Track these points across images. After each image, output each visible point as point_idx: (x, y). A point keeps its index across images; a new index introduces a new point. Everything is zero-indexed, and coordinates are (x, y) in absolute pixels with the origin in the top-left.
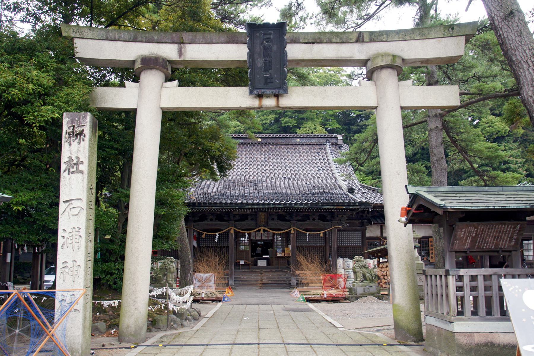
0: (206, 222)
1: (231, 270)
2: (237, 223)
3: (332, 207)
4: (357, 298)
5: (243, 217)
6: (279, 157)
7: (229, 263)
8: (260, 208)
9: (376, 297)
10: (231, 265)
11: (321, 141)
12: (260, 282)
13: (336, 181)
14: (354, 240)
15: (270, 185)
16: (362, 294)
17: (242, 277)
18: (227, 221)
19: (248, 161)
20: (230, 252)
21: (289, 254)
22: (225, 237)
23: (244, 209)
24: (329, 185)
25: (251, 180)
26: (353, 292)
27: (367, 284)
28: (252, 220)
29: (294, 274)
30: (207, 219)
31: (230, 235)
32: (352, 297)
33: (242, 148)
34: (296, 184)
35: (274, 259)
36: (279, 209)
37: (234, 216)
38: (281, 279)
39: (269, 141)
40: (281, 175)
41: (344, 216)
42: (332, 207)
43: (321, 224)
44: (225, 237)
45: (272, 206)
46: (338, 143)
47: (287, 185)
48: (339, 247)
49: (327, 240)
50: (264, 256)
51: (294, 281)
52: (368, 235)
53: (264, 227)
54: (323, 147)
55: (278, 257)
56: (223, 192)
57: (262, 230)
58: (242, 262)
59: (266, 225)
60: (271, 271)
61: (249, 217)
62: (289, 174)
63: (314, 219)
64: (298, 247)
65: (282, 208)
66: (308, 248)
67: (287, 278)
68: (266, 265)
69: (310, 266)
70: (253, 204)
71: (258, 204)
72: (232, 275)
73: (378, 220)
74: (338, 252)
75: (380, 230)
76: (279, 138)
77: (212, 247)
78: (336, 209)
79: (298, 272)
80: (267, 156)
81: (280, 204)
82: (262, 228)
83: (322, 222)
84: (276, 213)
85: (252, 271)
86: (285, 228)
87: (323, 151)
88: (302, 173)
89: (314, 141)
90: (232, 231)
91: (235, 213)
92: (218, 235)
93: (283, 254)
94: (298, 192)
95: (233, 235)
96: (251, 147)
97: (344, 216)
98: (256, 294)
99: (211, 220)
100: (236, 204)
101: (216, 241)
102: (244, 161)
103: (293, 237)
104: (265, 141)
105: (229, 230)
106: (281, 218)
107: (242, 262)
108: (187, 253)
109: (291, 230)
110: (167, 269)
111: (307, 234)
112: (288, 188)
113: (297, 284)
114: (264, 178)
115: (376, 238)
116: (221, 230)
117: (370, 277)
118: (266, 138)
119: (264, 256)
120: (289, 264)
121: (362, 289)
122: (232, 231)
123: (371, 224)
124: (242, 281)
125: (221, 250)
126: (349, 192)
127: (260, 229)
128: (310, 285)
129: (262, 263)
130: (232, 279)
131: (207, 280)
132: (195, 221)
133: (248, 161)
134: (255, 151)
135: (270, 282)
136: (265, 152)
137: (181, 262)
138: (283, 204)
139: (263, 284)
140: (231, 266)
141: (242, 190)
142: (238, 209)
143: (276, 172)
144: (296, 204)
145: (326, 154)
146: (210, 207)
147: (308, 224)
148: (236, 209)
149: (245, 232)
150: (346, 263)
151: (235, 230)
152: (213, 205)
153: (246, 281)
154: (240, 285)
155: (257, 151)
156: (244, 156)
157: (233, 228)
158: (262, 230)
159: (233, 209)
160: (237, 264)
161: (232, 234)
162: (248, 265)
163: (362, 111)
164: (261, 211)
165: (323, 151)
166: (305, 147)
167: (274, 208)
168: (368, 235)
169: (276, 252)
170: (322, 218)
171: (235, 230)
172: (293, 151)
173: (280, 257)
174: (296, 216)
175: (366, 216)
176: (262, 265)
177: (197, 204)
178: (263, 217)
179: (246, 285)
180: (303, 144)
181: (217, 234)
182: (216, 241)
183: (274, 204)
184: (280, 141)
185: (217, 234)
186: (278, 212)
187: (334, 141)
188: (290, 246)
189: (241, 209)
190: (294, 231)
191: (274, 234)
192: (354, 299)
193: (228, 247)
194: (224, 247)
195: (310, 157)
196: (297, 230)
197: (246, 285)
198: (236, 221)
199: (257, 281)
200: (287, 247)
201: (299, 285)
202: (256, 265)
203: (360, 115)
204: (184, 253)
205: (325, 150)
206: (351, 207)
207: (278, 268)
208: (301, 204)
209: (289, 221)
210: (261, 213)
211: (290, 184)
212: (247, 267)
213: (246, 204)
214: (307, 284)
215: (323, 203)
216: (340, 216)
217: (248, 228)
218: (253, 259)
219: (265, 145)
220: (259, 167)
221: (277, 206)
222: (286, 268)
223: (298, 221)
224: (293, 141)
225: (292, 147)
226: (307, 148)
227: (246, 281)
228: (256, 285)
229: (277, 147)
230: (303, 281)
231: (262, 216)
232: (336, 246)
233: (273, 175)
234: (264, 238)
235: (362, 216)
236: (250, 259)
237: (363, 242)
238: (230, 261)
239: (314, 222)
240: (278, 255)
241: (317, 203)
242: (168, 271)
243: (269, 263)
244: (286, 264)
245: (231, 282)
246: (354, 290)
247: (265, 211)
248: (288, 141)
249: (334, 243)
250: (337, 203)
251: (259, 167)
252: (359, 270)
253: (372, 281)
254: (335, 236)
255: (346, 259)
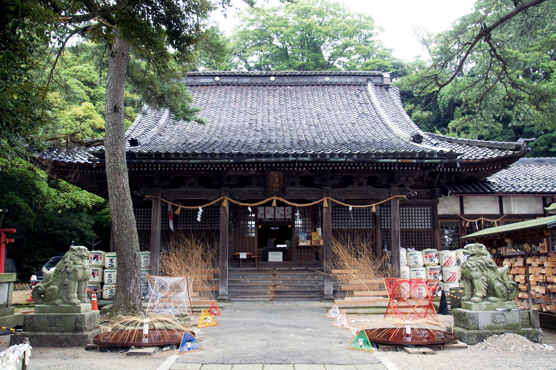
0: (183, 189)
1: (223, 268)
2: (234, 189)
3: (395, 161)
4: (481, 338)
5: (244, 181)
6: (300, 100)
7: (220, 257)
8: (271, 163)
9: (523, 334)
10: (223, 260)
11: (360, 80)
12: (273, 290)
13: (389, 129)
14: (420, 221)
15: (287, 134)
16: (490, 328)
17: (242, 280)
18: (217, 187)
19: (255, 106)
20: (221, 239)
21: (319, 242)
22: (212, 213)
23: (244, 163)
24: (379, 135)
25: (259, 129)
26: (470, 322)
27: (500, 306)
28: (258, 184)
29: (328, 277)
30: (184, 185)
31: (222, 210)
32: (469, 335)
33: (247, 89)
34: (327, 133)
35: (294, 250)
36: (303, 166)
37: (230, 178)
38: (307, 284)
39: (286, 80)
40: (304, 122)
41: (410, 179)
42: (395, 161)
43: (372, 191)
44: (212, 213)
45: (291, 159)
46: (384, 83)
47: (315, 135)
48: (402, 231)
49: (378, 220)
50: (278, 246)
51: (329, 288)
52: (441, 211)
53: (279, 196)
54: (362, 88)
55: (301, 247)
56: (212, 142)
57: (275, 202)
58: (243, 256)
59: (282, 192)
60: (290, 270)
61: (253, 180)
62: (316, 121)
63: (360, 184)
64: (334, 231)
65: (308, 162)
66: (351, 232)
67: (317, 282)
68: (281, 260)
69: (355, 261)
70: (259, 156)
71: (268, 155)
72: (224, 277)
73: (457, 188)
74: (402, 238)
75: (459, 205)
76: (300, 75)
77: (193, 230)
78: (399, 165)
79: (334, 271)
80: (283, 99)
81: (305, 155)
82: (275, 198)
83: (373, 188)
84: (297, 173)
85: (259, 271)
86: (313, 198)
87: (364, 92)
88: (335, 121)
89: (349, 80)
90: (225, 204)
91: (230, 173)
92: (201, 210)
93: (309, 242)
94: (333, 142)
95: (227, 210)
96: (260, 88)
97: (410, 179)
98: (263, 318)
99: (191, 185)
100: (231, 155)
101: (199, 219)
102: (249, 106)
103: (327, 213)
104: (280, 80)
105: (221, 202)
106: (307, 182)
107: (243, 256)
108: (130, 240)
109: (322, 202)
110: (68, 273)
111: (350, 209)
112: (316, 137)
113: (335, 292)
114: (279, 126)
115: (454, 217)
116: (207, 202)
117: (504, 289)
118: (281, 76)
119: (278, 246)
120: (318, 258)
121: (489, 316)
122: (225, 204)
123: (447, 195)
124: (242, 287)
125: (207, 235)
126: (414, 141)
127: (272, 200)
128: (356, 293)
129: (275, 257)
130: (225, 285)
131: (176, 288)
132: (164, 188)
133: (255, 106)
134: (266, 93)
135: (288, 288)
136: (280, 94)
137: (118, 257)
138: (311, 155)
139: (277, 292)
140: (223, 263)
141: (243, 140)
142: (234, 164)
143: (297, 119)
144: (332, 155)
145: (369, 97)
146: (186, 161)
147: (352, 191)
148: (230, 164)
149: (246, 204)
150: (412, 257)
151: (229, 202)
152: (191, 156)
153: (248, 287)
154: (239, 293)
155: (269, 93)
156: (249, 100)
157: (227, 198)
158: (275, 202)
159: (225, 164)
160: (235, 260)
161: (224, 208)
162: (254, 260)
163: (398, 68)
164: (274, 169)
165: (364, 92)
166: (337, 87)
167: (294, 162)
168: (441, 211)
169: (298, 238)
170: (373, 182)
171: (229, 202)
172: (321, 94)
173: (305, 247)
174: (331, 179)
175: (438, 182)
176: (275, 260)
177: (163, 156)
178: (277, 180)
179: (248, 293)
180: (334, 85)
181: (200, 208)
182: (199, 219)
183: (295, 155)
184: (302, 80)
185: (200, 208)
186: (301, 172)
187: (378, 80)
188: (319, 230)
189: (239, 164)
190: (328, 202)
191: (294, 209)
192: (474, 338)
193: (218, 231)
194: (213, 231)
195: (344, 100)
196: (333, 202)
197: (248, 293)
198: (231, 187)
199: (266, 287)
200: (315, 231)
201: (339, 295)
202: (266, 259)
203: (396, 72)
204: (125, 238)
205: (367, 91)
206: (426, 161)
207: (300, 265)
208: (341, 155)
209: (320, 186)
210: (272, 173)
211: (319, 134)
212: (252, 263)
213: (247, 154)
214: (351, 293)
215: (378, 154)
216: (403, 179)
217: (252, 198)
218: (262, 250)
219: (280, 86)
220: (272, 112)
221: (300, 159)
222: (314, 265)
223: (334, 187)
224: (320, 80)
225: (319, 88)
226: (341, 89)
227: (248, 287)
228: (265, 294)
229: (298, 88)
230: (344, 287)
231: (275, 178)
232: (398, 228)
233: (291, 122)
234: (278, 216)
235: (432, 183)
236: (256, 249)
237: (434, 222)
238: (221, 253)
239: (360, 188)
240: (301, 244)
241: (369, 154)
242: (72, 276)
243: (285, 258)
244: (314, 258)
245: (223, 290)
246: (472, 318)
247: (280, 170)
248: (313, 80)
249: (395, 222)
250: (402, 153)
251: (272, 112)
252: (479, 273)
253: (507, 297)
254: (396, 211)
255: (412, 251)
